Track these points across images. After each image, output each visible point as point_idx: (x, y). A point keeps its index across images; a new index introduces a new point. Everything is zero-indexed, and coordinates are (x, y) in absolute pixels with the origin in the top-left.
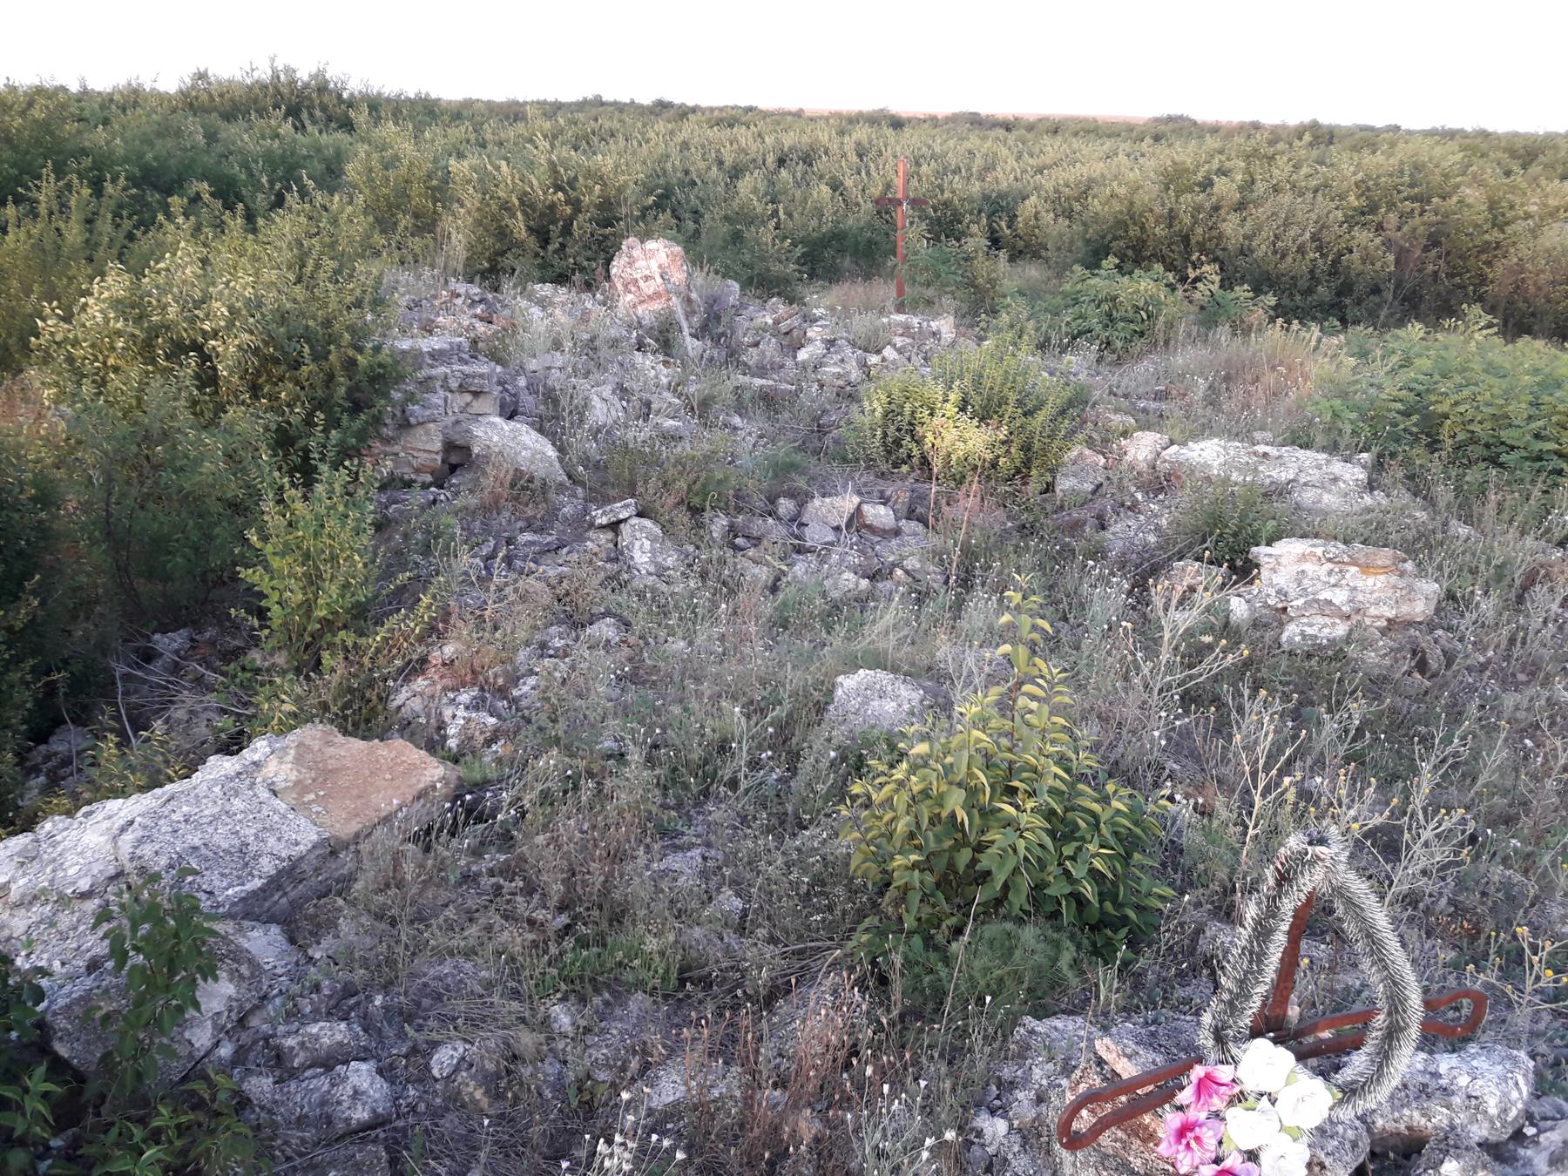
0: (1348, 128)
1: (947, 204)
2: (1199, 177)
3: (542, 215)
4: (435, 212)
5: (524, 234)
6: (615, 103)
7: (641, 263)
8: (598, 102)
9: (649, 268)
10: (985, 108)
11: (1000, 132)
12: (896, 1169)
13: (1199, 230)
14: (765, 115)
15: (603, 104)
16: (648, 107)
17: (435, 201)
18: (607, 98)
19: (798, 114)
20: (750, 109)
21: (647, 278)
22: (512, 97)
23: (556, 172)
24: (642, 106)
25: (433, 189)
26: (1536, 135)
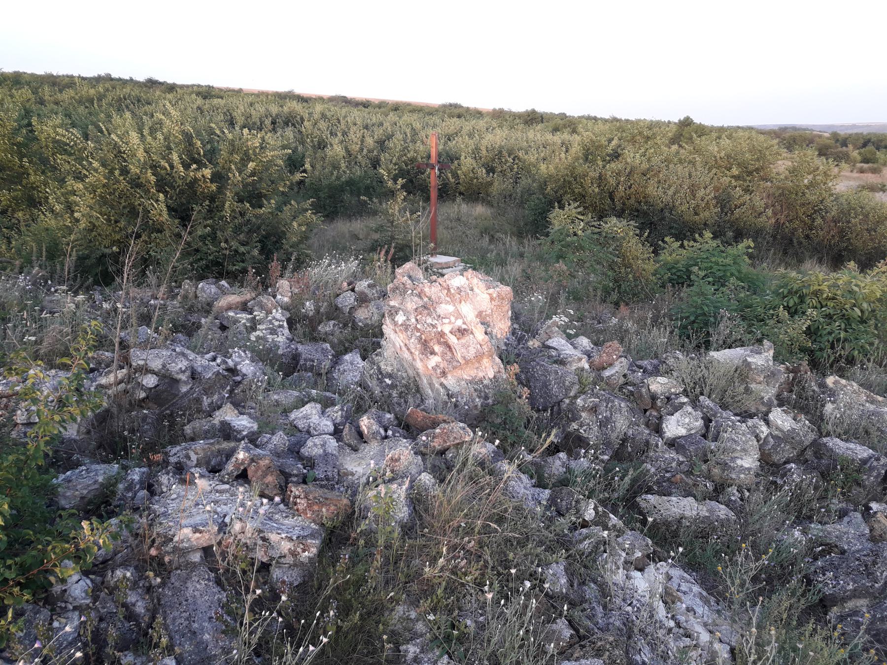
0: (221, 90)
1: (413, 160)
2: (609, 150)
3: (182, 192)
4: (22, 166)
5: (165, 215)
6: (120, 80)
7: (445, 308)
8: (108, 78)
9: (459, 315)
10: (349, 95)
11: (361, 107)
12: (45, 661)
13: (621, 188)
14: (182, 87)
15: (112, 79)
16: (143, 83)
17: (21, 156)
18: (115, 75)
19: (240, 91)
20: (152, 83)
21: (462, 332)
22: (48, 71)
23: (191, 144)
24: (139, 82)
25: (19, 145)
26: (573, 117)
